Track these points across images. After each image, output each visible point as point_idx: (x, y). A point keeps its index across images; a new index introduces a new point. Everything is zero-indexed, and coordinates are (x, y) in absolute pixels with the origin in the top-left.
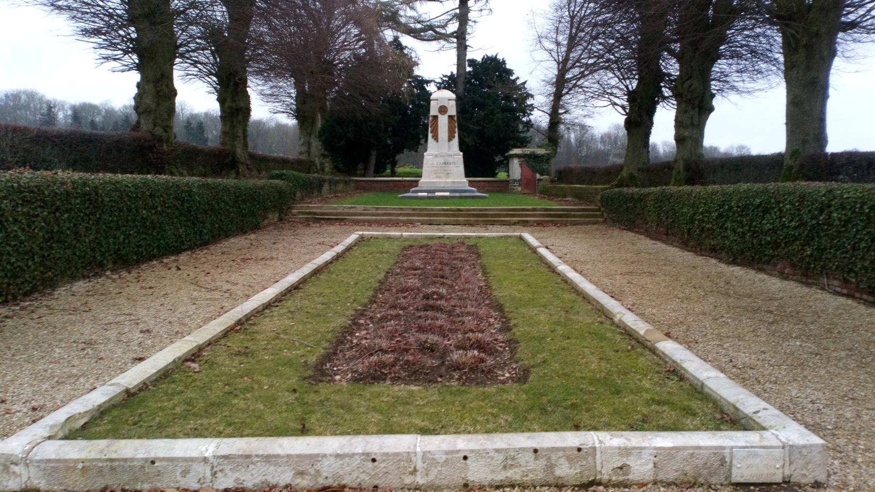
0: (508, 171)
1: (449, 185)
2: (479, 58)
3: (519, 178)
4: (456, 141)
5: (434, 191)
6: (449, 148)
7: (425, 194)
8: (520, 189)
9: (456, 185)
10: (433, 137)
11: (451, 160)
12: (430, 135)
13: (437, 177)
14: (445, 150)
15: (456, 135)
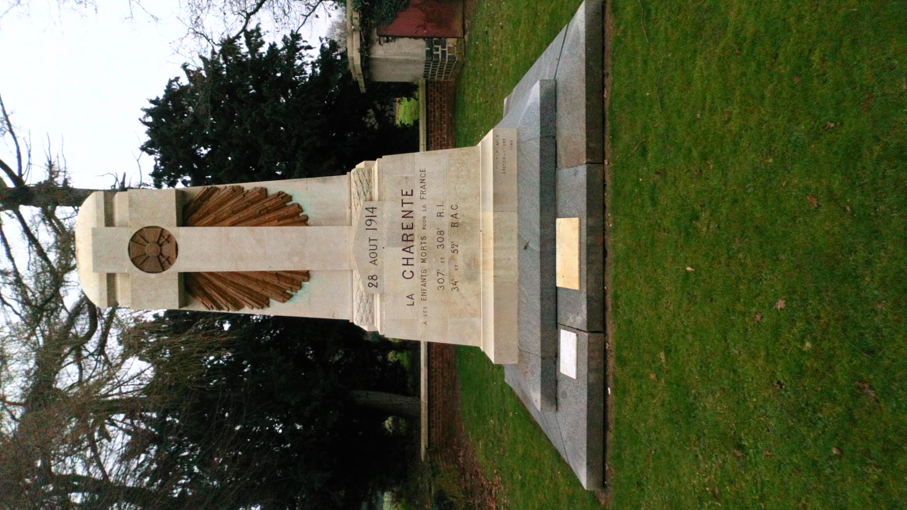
0: (388, 245)
1: (512, 220)
2: (150, 162)
3: (422, 42)
4: (303, 191)
5: (551, 295)
6: (333, 220)
7: (569, 346)
8: (451, 42)
9: (512, 187)
10: (286, 297)
11: (389, 213)
12: (277, 309)
13: (472, 276)
14: (347, 240)
15: (274, 187)
